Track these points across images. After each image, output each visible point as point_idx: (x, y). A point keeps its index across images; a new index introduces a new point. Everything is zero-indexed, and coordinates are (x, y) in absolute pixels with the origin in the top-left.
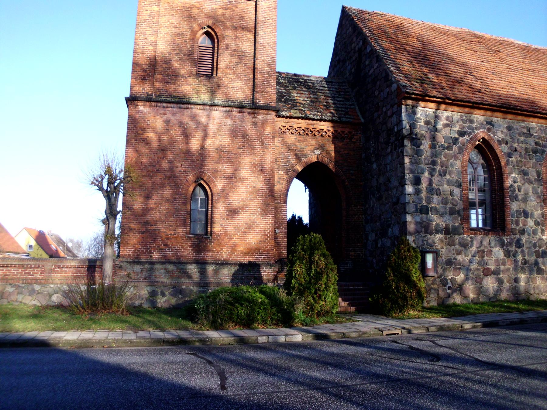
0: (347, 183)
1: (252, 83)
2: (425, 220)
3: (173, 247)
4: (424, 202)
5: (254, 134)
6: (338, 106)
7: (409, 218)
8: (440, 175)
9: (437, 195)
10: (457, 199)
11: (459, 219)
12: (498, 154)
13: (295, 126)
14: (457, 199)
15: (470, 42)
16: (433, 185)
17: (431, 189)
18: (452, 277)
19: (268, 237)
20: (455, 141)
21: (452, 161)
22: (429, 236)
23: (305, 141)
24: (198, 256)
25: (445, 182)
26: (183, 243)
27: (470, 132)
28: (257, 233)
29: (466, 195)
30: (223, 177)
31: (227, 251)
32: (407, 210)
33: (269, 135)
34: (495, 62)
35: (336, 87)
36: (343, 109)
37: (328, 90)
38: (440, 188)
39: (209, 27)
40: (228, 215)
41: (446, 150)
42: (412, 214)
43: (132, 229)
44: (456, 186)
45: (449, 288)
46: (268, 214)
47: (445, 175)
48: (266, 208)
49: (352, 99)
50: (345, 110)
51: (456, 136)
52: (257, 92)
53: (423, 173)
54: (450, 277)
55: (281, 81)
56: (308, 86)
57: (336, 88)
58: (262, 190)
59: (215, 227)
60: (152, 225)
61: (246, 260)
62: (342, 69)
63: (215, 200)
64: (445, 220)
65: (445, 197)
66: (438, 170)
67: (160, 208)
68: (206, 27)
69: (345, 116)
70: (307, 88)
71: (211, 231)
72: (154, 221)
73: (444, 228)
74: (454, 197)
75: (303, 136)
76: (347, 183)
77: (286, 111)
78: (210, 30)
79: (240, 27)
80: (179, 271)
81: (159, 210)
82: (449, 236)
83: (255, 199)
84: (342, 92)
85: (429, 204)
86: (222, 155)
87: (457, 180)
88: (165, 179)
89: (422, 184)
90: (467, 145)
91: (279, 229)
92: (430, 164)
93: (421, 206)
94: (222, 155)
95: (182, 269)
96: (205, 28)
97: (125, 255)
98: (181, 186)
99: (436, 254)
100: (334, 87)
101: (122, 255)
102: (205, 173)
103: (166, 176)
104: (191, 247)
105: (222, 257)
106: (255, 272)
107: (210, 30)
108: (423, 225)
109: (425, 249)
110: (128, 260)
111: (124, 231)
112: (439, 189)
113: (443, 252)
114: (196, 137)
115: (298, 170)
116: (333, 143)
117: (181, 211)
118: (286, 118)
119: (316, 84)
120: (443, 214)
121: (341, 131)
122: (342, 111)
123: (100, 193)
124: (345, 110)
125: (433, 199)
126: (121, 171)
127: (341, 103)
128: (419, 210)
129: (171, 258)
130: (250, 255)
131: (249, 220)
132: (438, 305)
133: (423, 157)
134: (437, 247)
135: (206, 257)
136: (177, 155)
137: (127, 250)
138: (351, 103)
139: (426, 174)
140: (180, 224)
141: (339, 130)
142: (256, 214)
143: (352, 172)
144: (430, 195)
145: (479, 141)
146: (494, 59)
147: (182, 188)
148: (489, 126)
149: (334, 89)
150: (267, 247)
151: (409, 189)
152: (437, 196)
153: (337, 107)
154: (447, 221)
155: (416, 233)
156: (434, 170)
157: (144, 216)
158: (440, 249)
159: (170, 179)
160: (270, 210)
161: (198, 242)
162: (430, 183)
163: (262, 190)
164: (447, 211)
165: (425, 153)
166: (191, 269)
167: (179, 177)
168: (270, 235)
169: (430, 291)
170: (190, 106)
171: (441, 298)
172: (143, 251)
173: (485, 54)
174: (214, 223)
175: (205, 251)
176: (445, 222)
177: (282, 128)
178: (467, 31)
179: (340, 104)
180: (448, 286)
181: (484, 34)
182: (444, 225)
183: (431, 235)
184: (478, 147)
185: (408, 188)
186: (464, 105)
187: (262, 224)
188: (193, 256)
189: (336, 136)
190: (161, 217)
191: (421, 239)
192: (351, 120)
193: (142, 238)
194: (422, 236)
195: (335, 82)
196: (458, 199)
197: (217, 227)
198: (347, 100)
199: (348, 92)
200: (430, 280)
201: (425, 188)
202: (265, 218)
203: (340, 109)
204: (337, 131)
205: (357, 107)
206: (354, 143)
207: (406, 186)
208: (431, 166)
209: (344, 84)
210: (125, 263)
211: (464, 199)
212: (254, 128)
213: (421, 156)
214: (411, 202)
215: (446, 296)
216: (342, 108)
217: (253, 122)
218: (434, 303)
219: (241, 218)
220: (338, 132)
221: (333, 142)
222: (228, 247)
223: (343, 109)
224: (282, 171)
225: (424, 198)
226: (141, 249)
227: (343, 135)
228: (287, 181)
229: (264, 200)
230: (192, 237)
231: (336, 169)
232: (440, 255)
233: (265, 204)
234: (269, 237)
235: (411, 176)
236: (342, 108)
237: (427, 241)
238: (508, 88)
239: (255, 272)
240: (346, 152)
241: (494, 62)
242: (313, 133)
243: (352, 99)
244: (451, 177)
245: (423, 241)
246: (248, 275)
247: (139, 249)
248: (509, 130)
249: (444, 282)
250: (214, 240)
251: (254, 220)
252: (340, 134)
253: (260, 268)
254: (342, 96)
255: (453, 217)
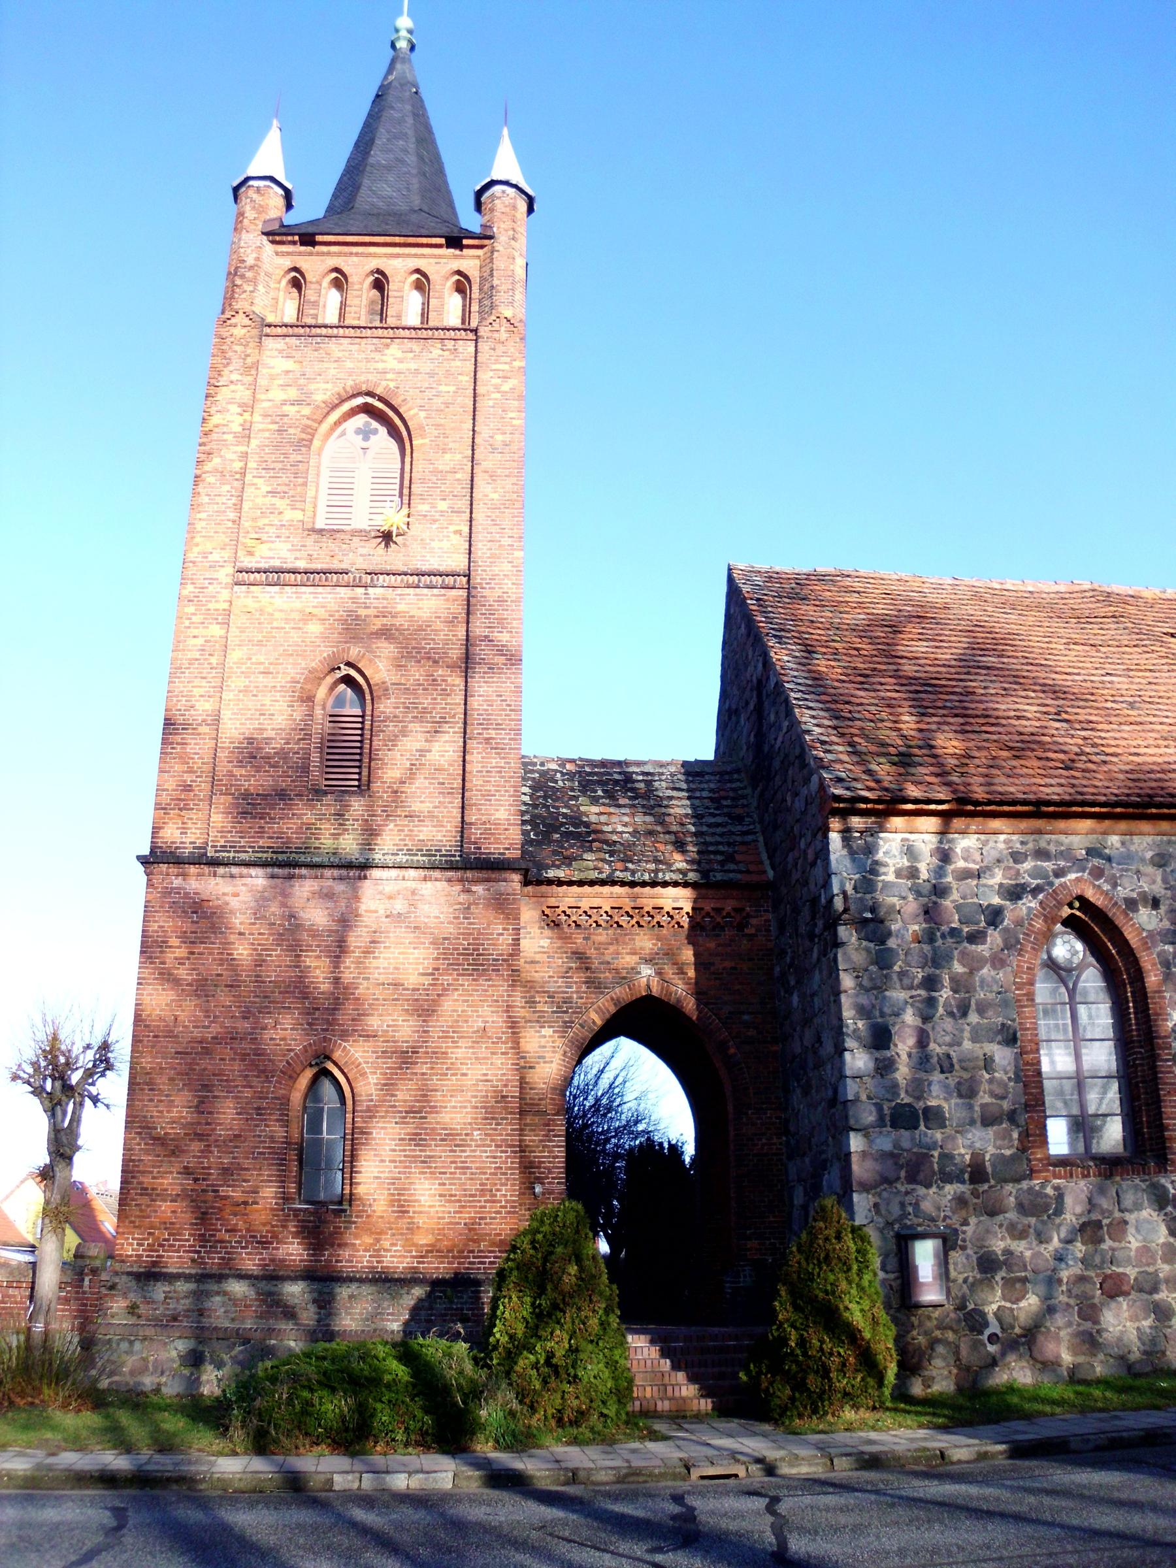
0: (732, 1051)
1: (458, 801)
2: (906, 1144)
3: (251, 1237)
4: (903, 1095)
5: (463, 934)
6: (708, 839)
7: (856, 1143)
8: (951, 1014)
9: (942, 1072)
10: (1005, 1078)
11: (1015, 1135)
12: (1129, 937)
13: (585, 904)
14: (1005, 1078)
15: (1083, 619)
16: (928, 1044)
17: (923, 1060)
18: (999, 1307)
19: (501, 1207)
20: (995, 916)
21: (985, 971)
22: (921, 1191)
23: (611, 944)
24: (316, 1261)
25: (967, 1034)
26: (277, 1226)
27: (1038, 885)
28: (471, 1196)
29: (1032, 1064)
30: (383, 1052)
31: (393, 1245)
32: (852, 1122)
33: (502, 934)
34: (1151, 671)
35: (712, 786)
36: (721, 848)
37: (689, 798)
38: (952, 1053)
39: (349, 664)
40: (394, 1150)
41: (966, 944)
42: (863, 1130)
43: (146, 1189)
44: (999, 1043)
45: (993, 1338)
46: (501, 1146)
47: (965, 1014)
48: (495, 1129)
49: (751, 817)
50: (726, 848)
51: (996, 900)
52: (471, 824)
53: (897, 1015)
54: (994, 1307)
55: (560, 783)
56: (633, 790)
57: (711, 791)
58: (487, 1081)
59: (359, 1184)
60: (198, 1179)
61: (439, 1268)
62: (735, 736)
63: (361, 1111)
64: (969, 1142)
65: (966, 1075)
66: (942, 1000)
67: (220, 1135)
68: (342, 666)
69: (723, 866)
70: (630, 798)
71: (351, 1194)
72: (203, 1168)
73: (969, 1166)
74: (996, 1074)
75: (605, 929)
76: (732, 1051)
77: (558, 867)
78: (353, 673)
79: (429, 658)
80: (262, 1300)
81: (217, 1141)
82: (986, 1186)
83: (465, 1107)
84: (726, 798)
85: (919, 1098)
86: (381, 994)
87: (1003, 1025)
88: (234, 1060)
89: (896, 1045)
90: (1030, 924)
91: (543, 1184)
92: (918, 987)
93: (894, 1108)
94: (381, 994)
95: (270, 1294)
96: (339, 668)
97: (127, 1256)
98: (273, 1077)
99: (948, 1243)
100: (706, 786)
101: (121, 1255)
102: (336, 1042)
103: (235, 1054)
104: (296, 1235)
105: (378, 1262)
106: (466, 1303)
107: (353, 673)
108: (902, 1161)
109: (911, 1227)
110: (135, 1270)
111: (128, 1193)
112: (948, 1056)
113: (969, 1234)
114: (313, 951)
115: (594, 1022)
116: (689, 943)
117: (273, 1142)
118: (558, 885)
119: (656, 784)
120: (963, 1125)
121: (713, 909)
122: (715, 853)
123: (36, 1101)
124: (726, 848)
125: (930, 1084)
126: (88, 1047)
127: (719, 830)
128: (888, 1118)
129: (244, 1265)
130: (453, 1257)
131: (452, 1162)
132: (960, 1389)
133: (896, 968)
134: (948, 1221)
135: (337, 1261)
136: (266, 997)
137: (132, 1244)
138: (745, 828)
139: (910, 1017)
140: (268, 1176)
141: (708, 906)
142: (470, 1146)
143: (746, 1017)
144: (923, 1075)
145: (1071, 906)
146: (1151, 660)
147: (277, 1082)
148: (1096, 862)
149: (705, 794)
150: (500, 1235)
151: (858, 1060)
152: (942, 1076)
153: (705, 843)
154: (978, 1145)
155: (881, 1184)
156: (931, 1002)
157: (178, 1156)
158: (957, 1226)
159: (244, 1060)
160: (507, 1135)
161: (314, 1222)
162: (923, 1041)
163: (487, 1081)
164: (976, 1116)
165: (902, 957)
166: (293, 1295)
167: (269, 1055)
168: (507, 1201)
169: (933, 1349)
170: (297, 871)
171: (968, 1369)
172: (174, 1246)
173: (1127, 649)
174: (356, 1172)
175: (332, 1245)
176: (970, 1147)
177: (547, 911)
178: (1087, 586)
179: (714, 834)
180: (987, 1332)
181: (1138, 588)
182: (968, 1157)
183: (928, 1186)
184: (1071, 923)
185: (853, 1058)
186: (916, 810)
187: (485, 1173)
188: (301, 1261)
189: (698, 923)
190: (220, 1158)
191: (898, 1199)
192: (739, 876)
193: (173, 1212)
194: (899, 1192)
195: (711, 774)
196: (1009, 1079)
197: (365, 1183)
198: (739, 819)
199: (744, 797)
200: (929, 1318)
201: (904, 1057)
202: (495, 1157)
203: (711, 848)
204: (702, 909)
205: (761, 839)
206: (751, 937)
207: (847, 1055)
208: (923, 993)
209: (735, 776)
210: (124, 1278)
211: (1026, 1076)
212: (465, 918)
213: (890, 967)
214: (864, 1097)
215: (982, 1364)
216: (718, 843)
217: (460, 903)
218: (944, 1383)
219: (430, 1157)
220: (703, 913)
221: (692, 939)
222: (394, 1235)
223: (721, 848)
224: (550, 1027)
225: (902, 1083)
226: (168, 1240)
227: (719, 919)
228: (565, 1052)
229: (492, 1107)
230: (300, 1210)
231: (700, 1012)
232: (959, 1242)
233: (493, 1118)
234: (505, 1207)
235: (860, 1024)
236: (718, 843)
237: (916, 1205)
238: (1165, 743)
239: (466, 1303)
240: (728, 964)
241: (1146, 670)
242: (655, 920)
243: (751, 817)
244: (983, 1018)
245: (902, 1205)
246: (445, 1309)
247: (165, 1240)
248: (1160, 866)
249: (974, 1321)
250: (357, 1217)
251: (463, 1162)
252: (712, 917)
253: (480, 1292)
254: (725, 810)
255: (995, 1133)
